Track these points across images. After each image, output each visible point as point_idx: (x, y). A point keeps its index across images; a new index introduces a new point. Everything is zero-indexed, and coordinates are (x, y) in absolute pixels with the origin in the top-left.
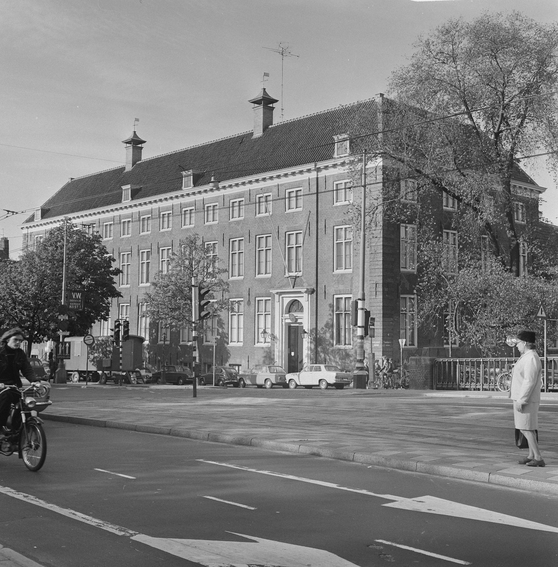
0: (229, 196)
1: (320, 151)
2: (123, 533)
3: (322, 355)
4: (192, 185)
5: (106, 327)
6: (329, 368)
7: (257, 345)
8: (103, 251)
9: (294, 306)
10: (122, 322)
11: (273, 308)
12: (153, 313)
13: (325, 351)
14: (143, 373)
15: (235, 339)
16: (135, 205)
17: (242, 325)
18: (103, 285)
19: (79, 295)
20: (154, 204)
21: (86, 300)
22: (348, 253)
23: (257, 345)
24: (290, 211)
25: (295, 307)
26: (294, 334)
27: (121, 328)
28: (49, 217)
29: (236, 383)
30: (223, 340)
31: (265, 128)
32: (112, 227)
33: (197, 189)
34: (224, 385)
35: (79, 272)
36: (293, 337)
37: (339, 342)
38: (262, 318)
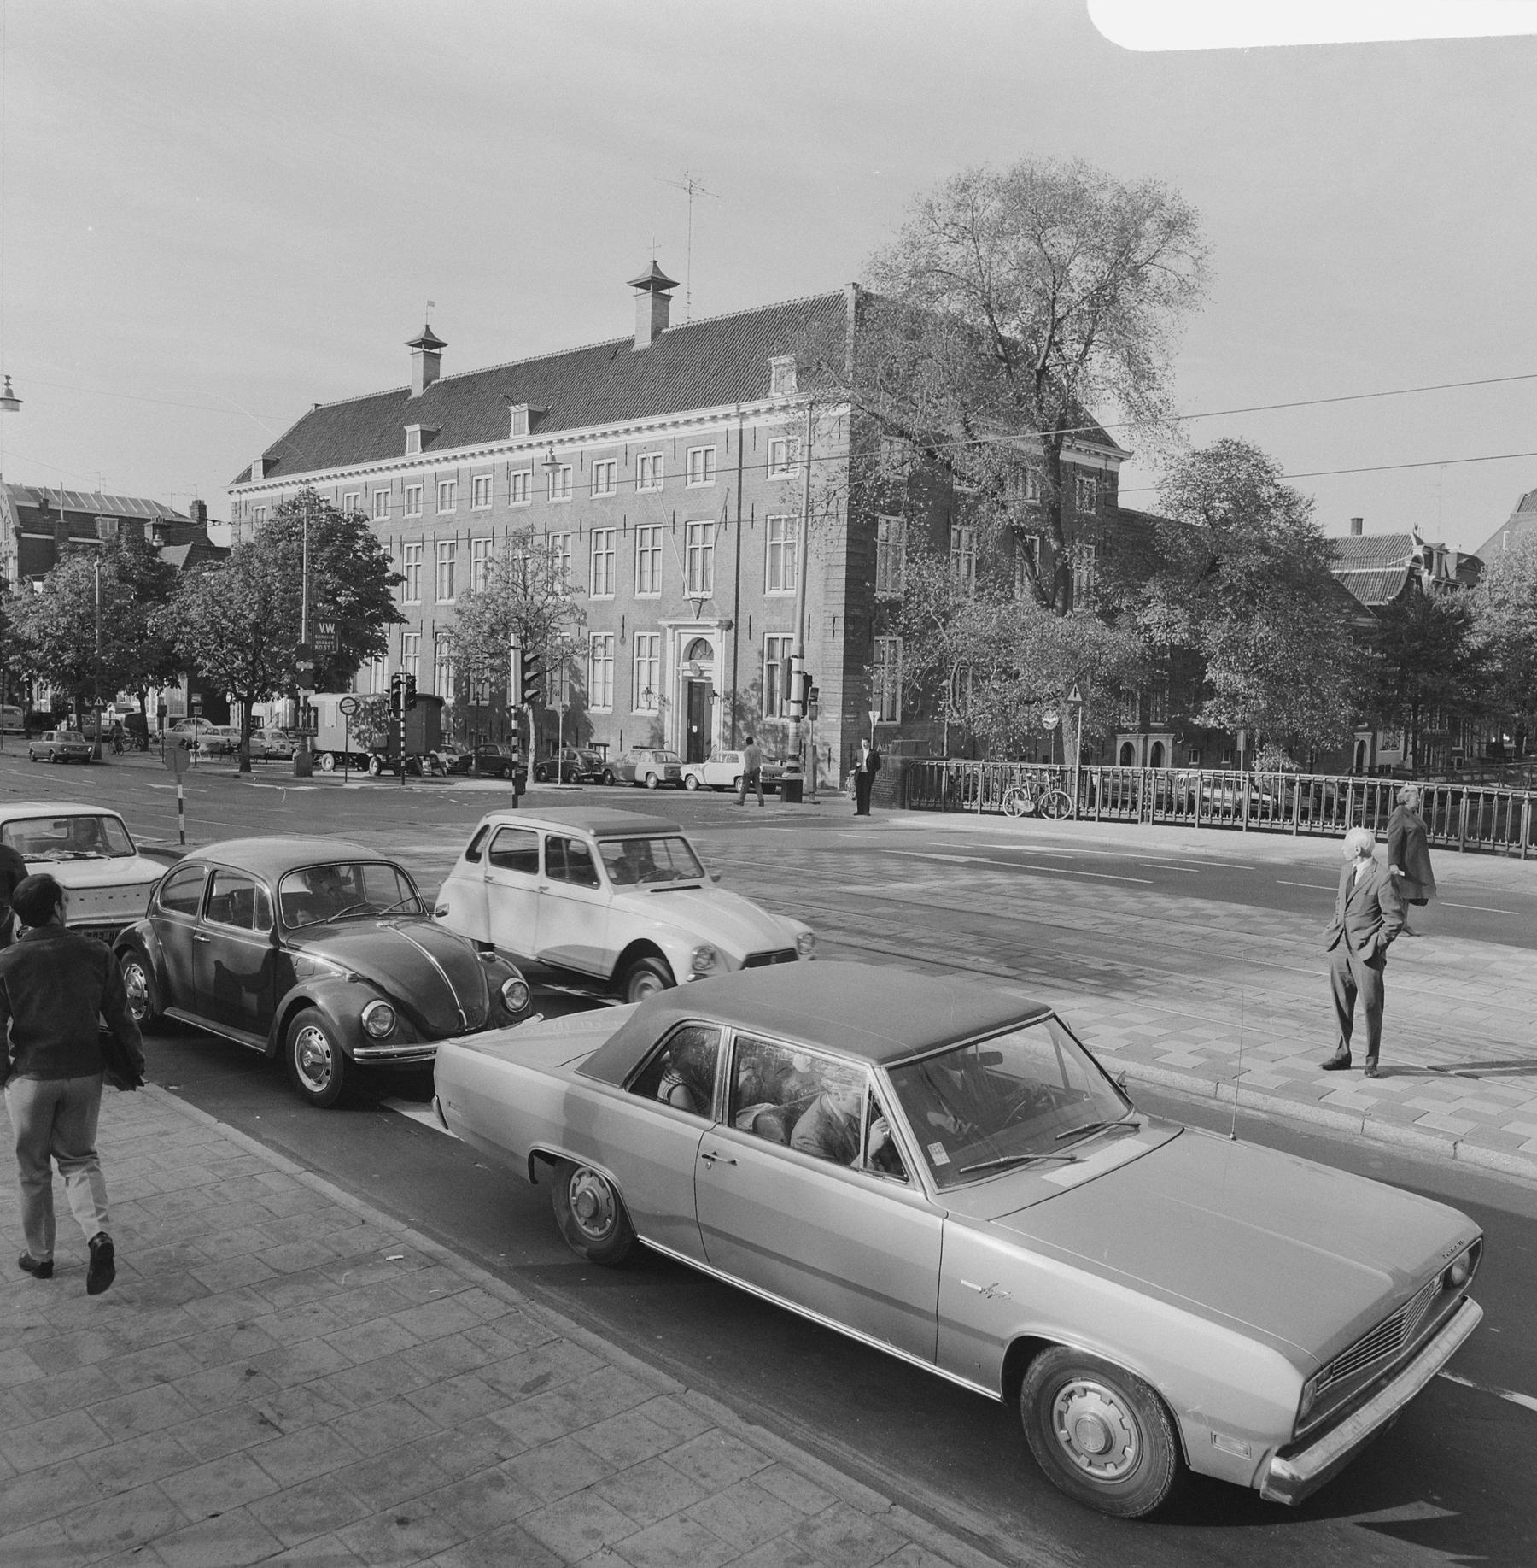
0: (591, 453)
1: (744, 383)
4: (527, 430)
7: (636, 712)
8: (372, 543)
9: (698, 647)
10: (403, 678)
11: (663, 651)
12: (457, 661)
13: (750, 727)
14: (443, 757)
15: (599, 700)
17: (610, 678)
18: (374, 605)
19: (331, 628)
20: (462, 461)
21: (344, 632)
22: (789, 563)
26: (697, 695)
27: (403, 688)
28: (278, 474)
29: (599, 775)
30: (580, 702)
31: (656, 333)
32: (389, 497)
33: (535, 439)
34: (580, 781)
36: (695, 699)
37: (771, 711)
38: (644, 667)
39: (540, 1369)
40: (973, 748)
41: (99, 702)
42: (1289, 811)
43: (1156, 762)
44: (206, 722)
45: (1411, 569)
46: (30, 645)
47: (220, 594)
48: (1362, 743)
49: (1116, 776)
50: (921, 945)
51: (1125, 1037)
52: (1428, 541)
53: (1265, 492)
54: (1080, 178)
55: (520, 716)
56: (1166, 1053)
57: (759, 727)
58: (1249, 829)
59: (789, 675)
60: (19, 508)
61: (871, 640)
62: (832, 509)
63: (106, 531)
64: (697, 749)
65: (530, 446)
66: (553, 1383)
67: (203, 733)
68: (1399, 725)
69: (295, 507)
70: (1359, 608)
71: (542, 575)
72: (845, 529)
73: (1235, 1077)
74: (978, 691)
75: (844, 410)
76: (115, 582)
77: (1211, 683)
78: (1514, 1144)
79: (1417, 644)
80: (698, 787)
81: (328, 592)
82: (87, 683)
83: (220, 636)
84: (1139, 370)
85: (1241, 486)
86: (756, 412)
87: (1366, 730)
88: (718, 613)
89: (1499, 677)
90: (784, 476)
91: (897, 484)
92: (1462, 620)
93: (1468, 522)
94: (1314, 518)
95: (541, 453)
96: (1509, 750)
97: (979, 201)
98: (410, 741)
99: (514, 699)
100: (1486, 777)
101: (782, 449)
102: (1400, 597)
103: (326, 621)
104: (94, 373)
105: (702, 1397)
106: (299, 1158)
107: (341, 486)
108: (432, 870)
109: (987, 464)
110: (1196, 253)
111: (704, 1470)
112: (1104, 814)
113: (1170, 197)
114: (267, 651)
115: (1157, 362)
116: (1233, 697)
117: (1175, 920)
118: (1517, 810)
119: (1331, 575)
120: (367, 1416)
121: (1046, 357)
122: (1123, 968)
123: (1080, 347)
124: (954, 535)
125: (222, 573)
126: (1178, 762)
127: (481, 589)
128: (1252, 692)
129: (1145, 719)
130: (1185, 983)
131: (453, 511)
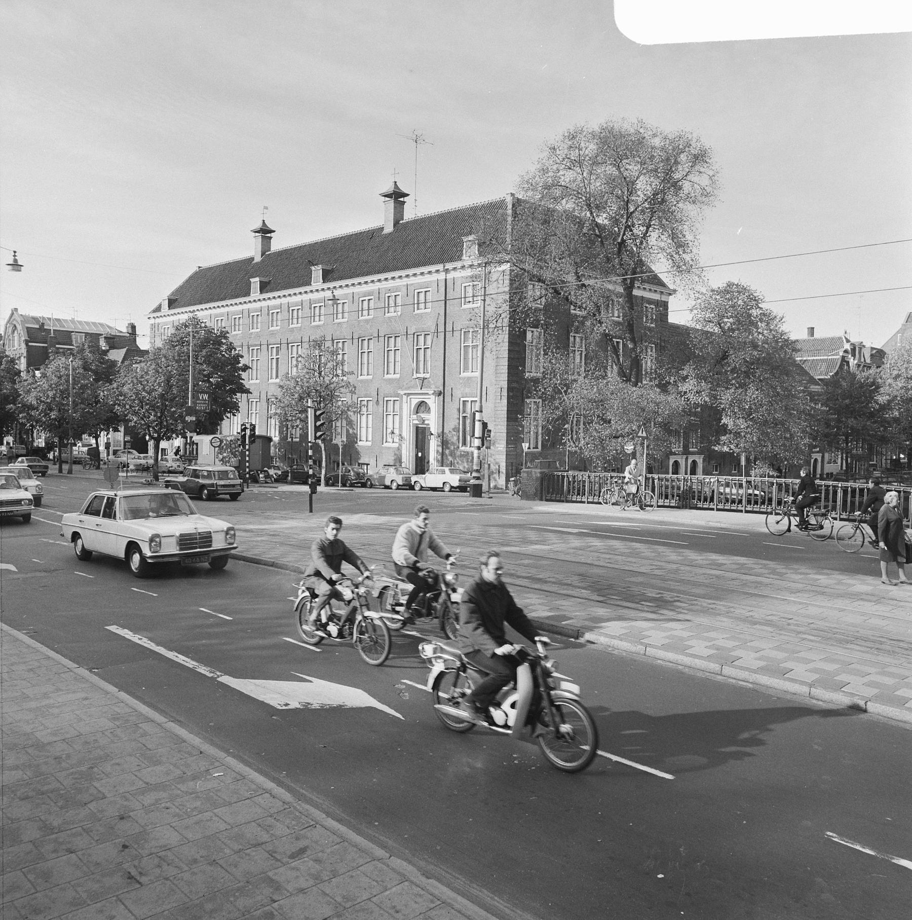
2: (212, 675)
3: (450, 458)
4: (321, 281)
5: (235, 422)
6: (452, 471)
8: (231, 347)
9: (422, 406)
10: (248, 426)
11: (401, 408)
13: (452, 454)
14: (272, 472)
15: (364, 438)
16: (264, 299)
17: (370, 425)
18: (231, 383)
19: (206, 397)
20: (283, 299)
21: (214, 399)
22: (475, 356)
23: (385, 445)
24: (419, 312)
25: (422, 408)
26: (421, 435)
27: (248, 432)
29: (364, 482)
30: (352, 440)
31: (396, 223)
33: (326, 286)
34: (352, 485)
35: (207, 369)
36: (420, 437)
37: (464, 444)
38: (390, 418)
39: (301, 844)
40: (583, 465)
41: (71, 441)
42: (770, 500)
43: (693, 472)
44: (134, 452)
45: (843, 357)
46: (31, 407)
47: (142, 377)
48: (816, 460)
49: (667, 480)
50: (546, 582)
51: (667, 637)
52: (853, 340)
53: (754, 312)
54: (642, 131)
55: (316, 447)
56: (692, 647)
57: (458, 453)
58: (747, 512)
59: (474, 422)
60: (27, 328)
61: (523, 401)
62: (499, 324)
63: (78, 340)
64: (421, 466)
65: (323, 290)
66: (309, 852)
67: (134, 459)
68: (837, 449)
69: (186, 326)
70: (812, 381)
71: (330, 365)
72: (507, 336)
73: (732, 661)
74: (586, 430)
75: (506, 267)
76: (81, 371)
77: (725, 426)
78: (902, 702)
79: (847, 401)
80: (422, 488)
81: (205, 376)
82: (66, 430)
83: (141, 402)
84: (680, 245)
85: (740, 311)
86: (455, 269)
87: (818, 452)
88: (433, 386)
89: (896, 420)
90: (470, 306)
91: (536, 310)
92: (874, 387)
93: (876, 331)
94: (784, 328)
95: (328, 294)
96: (904, 463)
97: (582, 145)
98: (254, 464)
99: (311, 438)
100: (890, 479)
101: (470, 290)
102: (836, 374)
103: (203, 392)
104: (77, 252)
105: (399, 861)
106: (166, 714)
107: (212, 315)
108: (259, 539)
109: (590, 298)
110: (711, 173)
111: (398, 908)
112: (748, 509)
113: (694, 140)
114: (169, 410)
115: (689, 237)
116: (737, 434)
117: (701, 567)
118: (835, 493)
119: (795, 361)
120: (194, 874)
121: (624, 234)
122: (667, 596)
123: (643, 229)
124: (572, 339)
125: (143, 364)
126: (706, 472)
127: (294, 373)
128: (749, 430)
129: (686, 447)
130: (705, 605)
131: (278, 328)
